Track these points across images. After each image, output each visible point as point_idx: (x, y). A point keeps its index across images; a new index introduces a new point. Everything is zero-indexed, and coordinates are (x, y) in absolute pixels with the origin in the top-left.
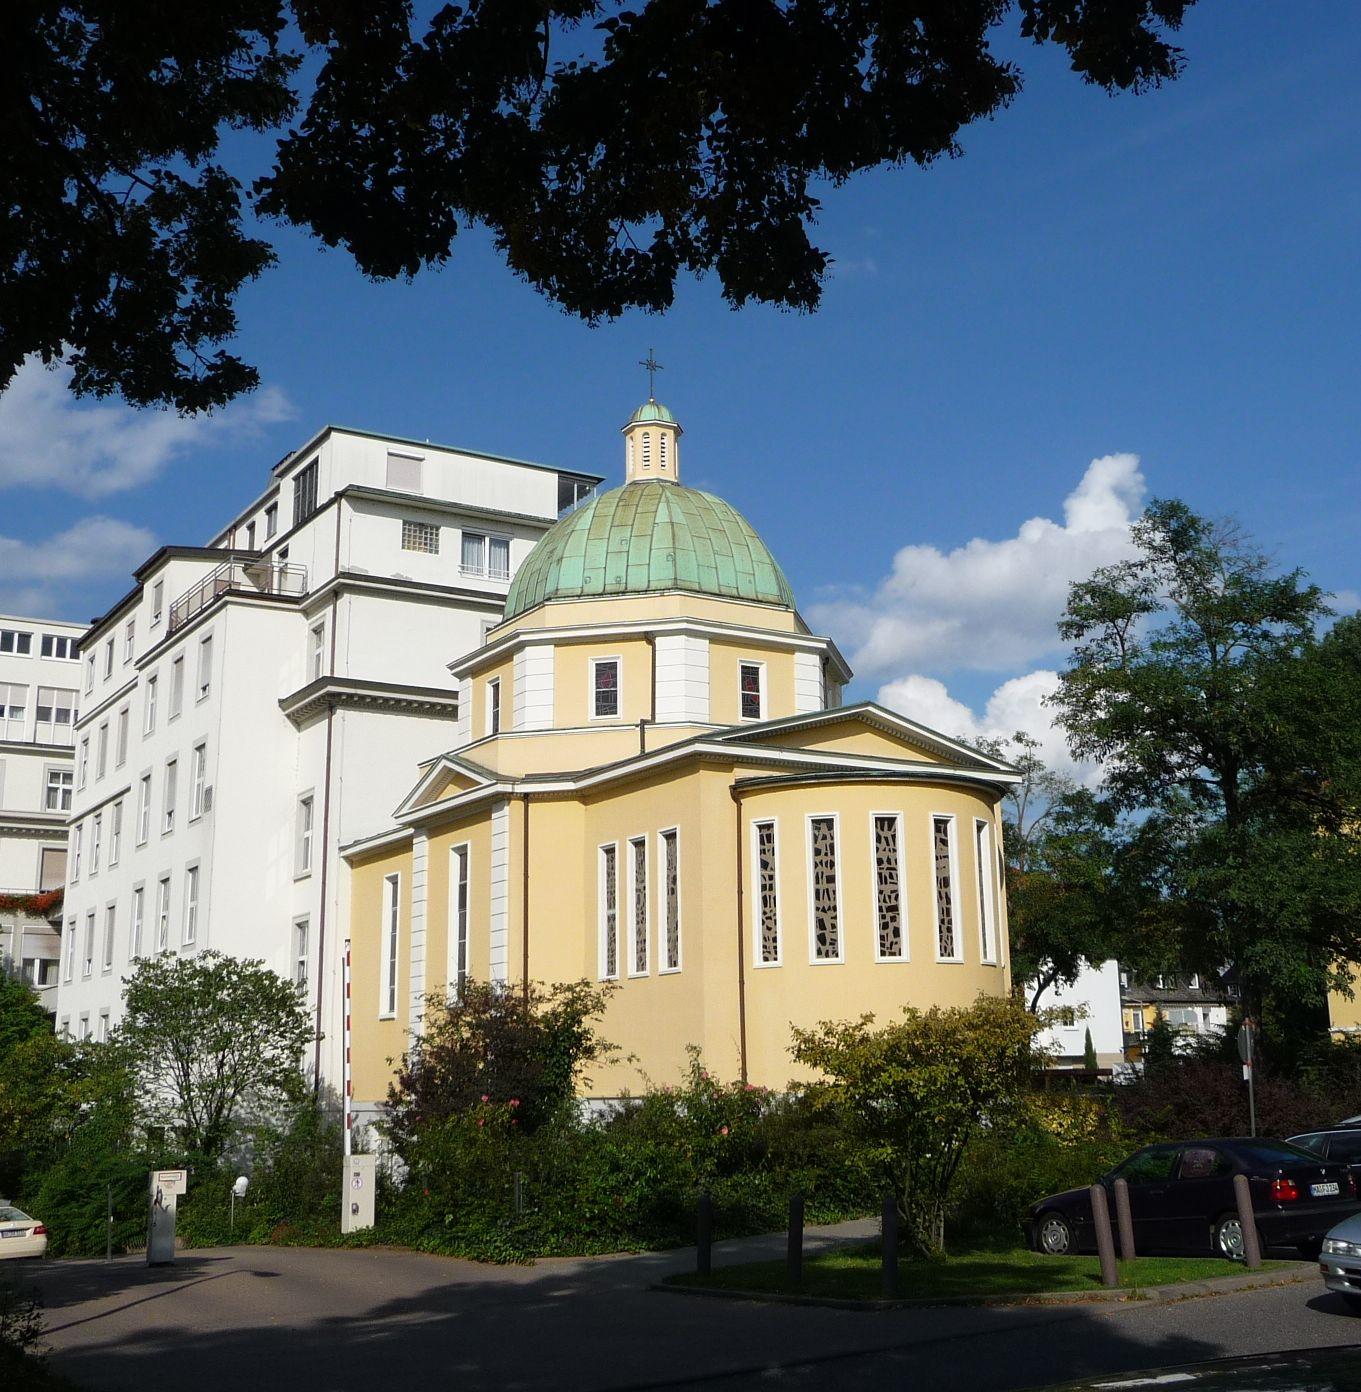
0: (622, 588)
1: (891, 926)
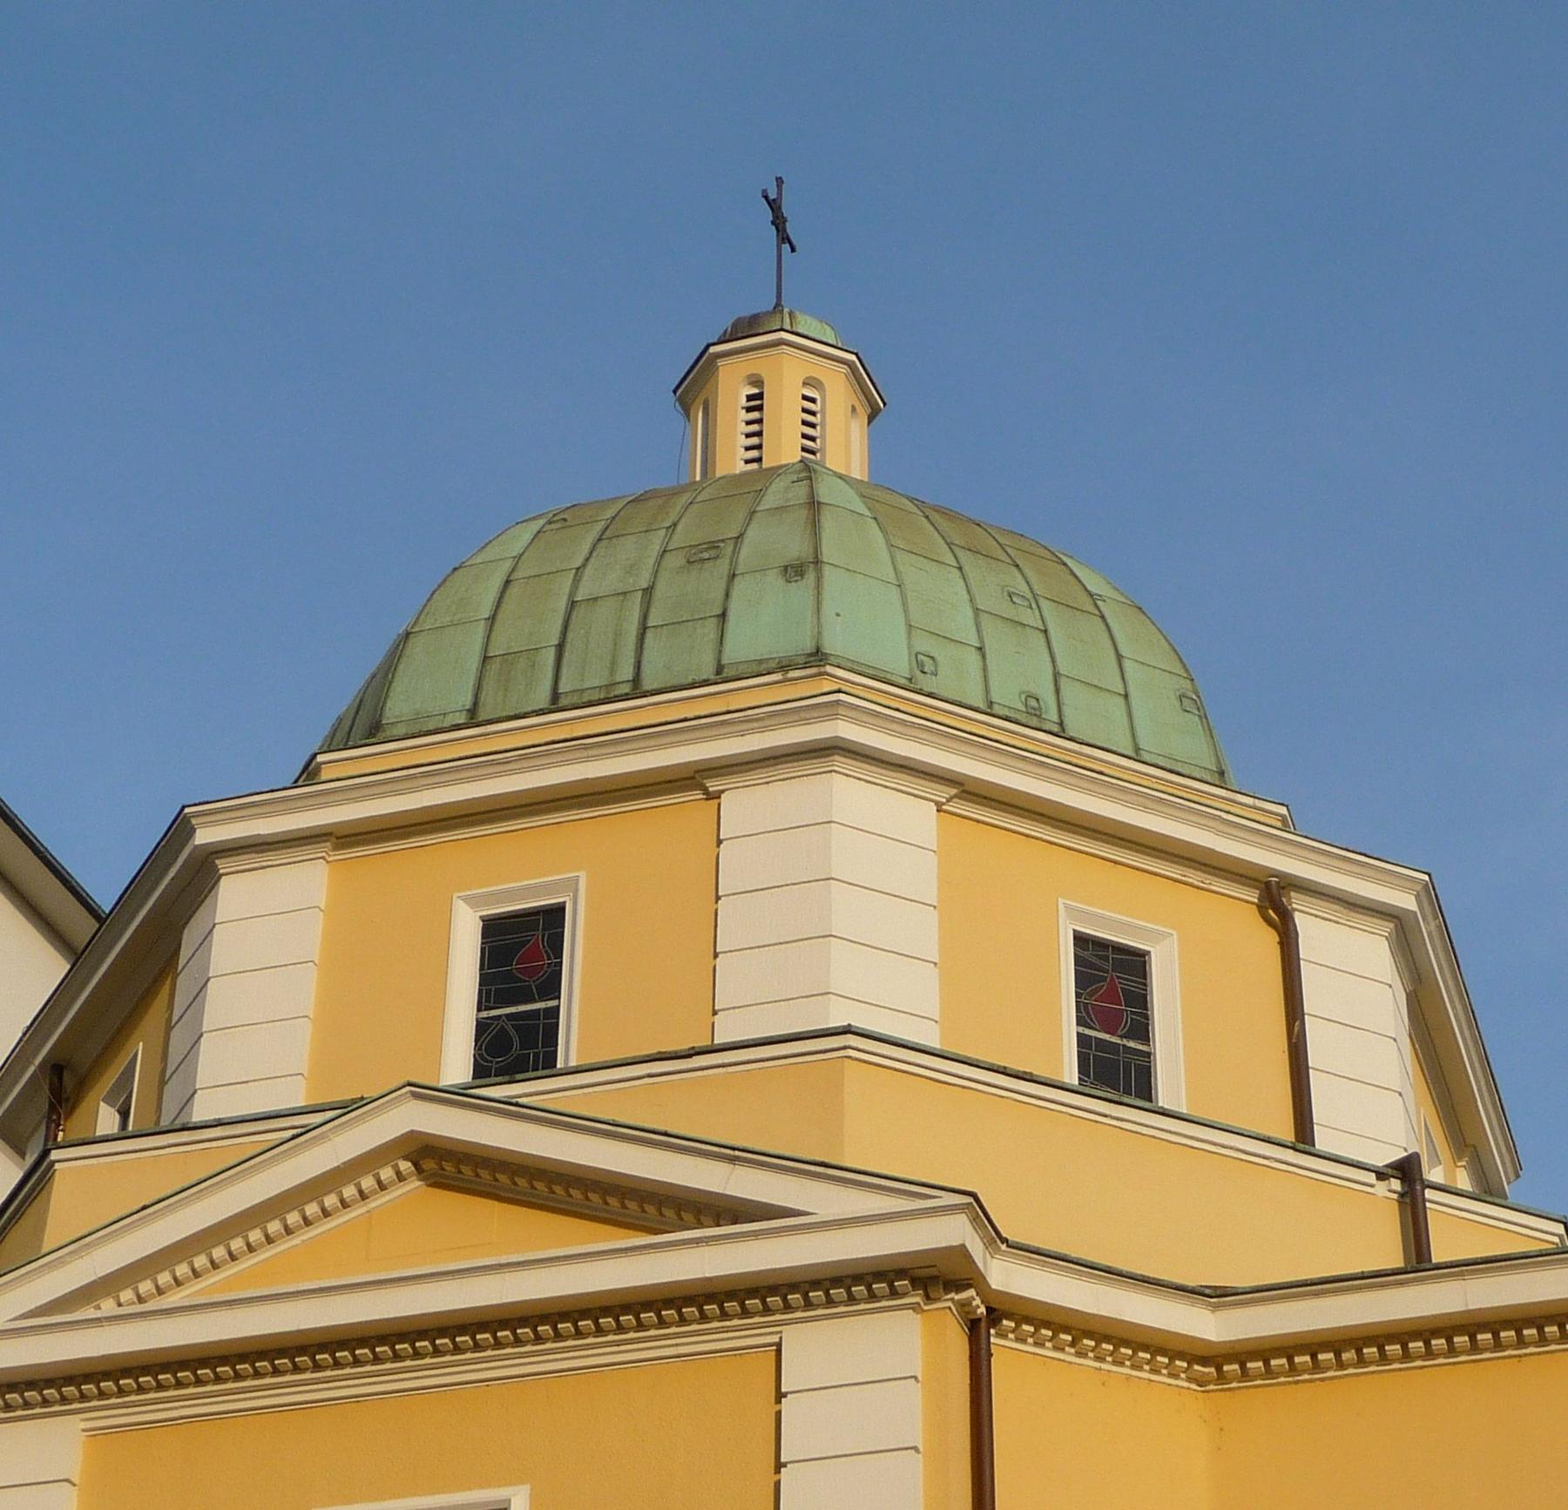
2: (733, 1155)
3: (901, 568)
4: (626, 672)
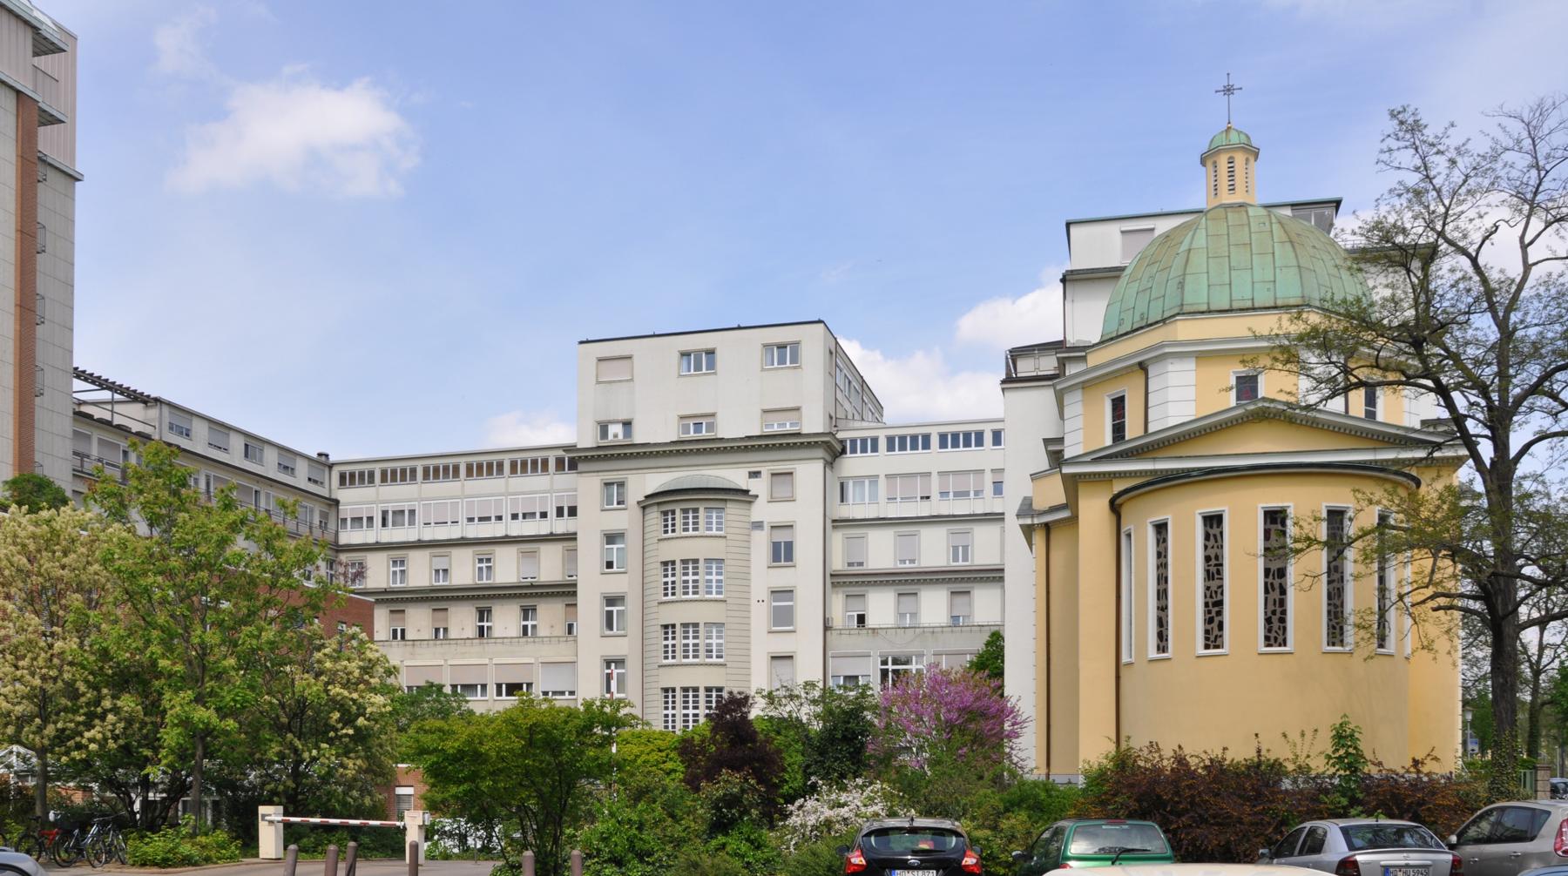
1: (1217, 620)
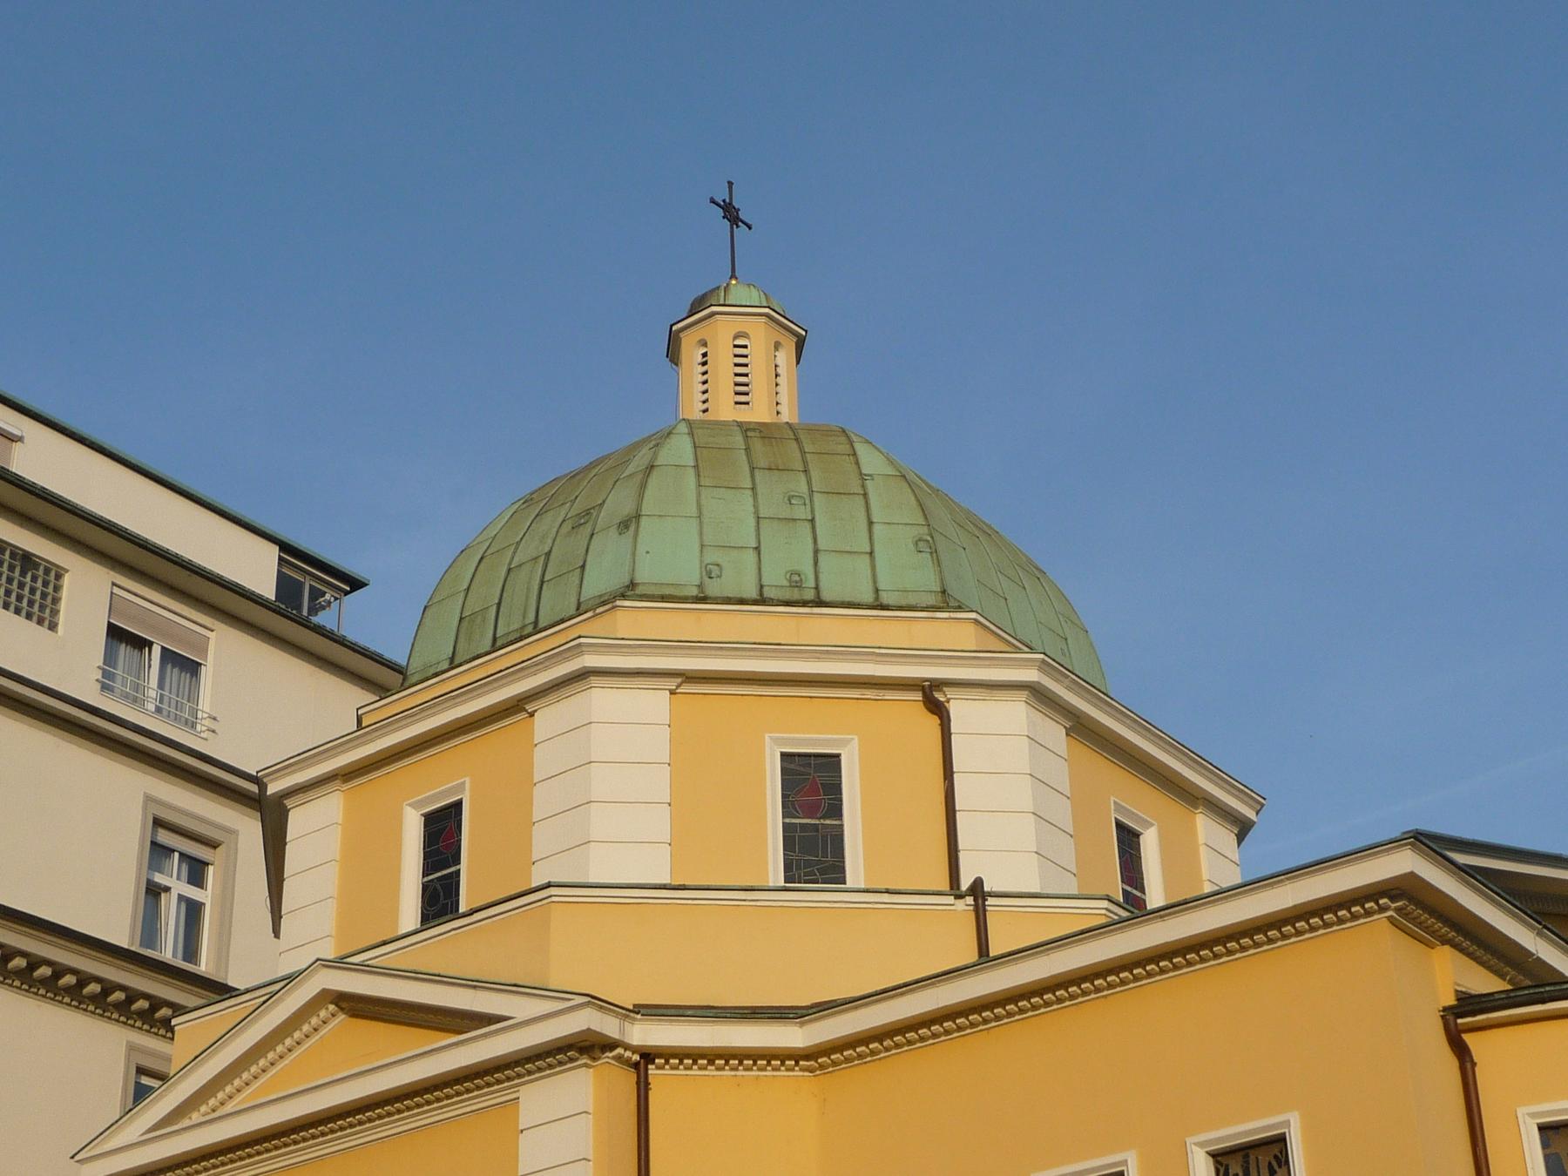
0: (809, 595)
2: (475, 984)
3: (703, 502)
4: (531, 617)
